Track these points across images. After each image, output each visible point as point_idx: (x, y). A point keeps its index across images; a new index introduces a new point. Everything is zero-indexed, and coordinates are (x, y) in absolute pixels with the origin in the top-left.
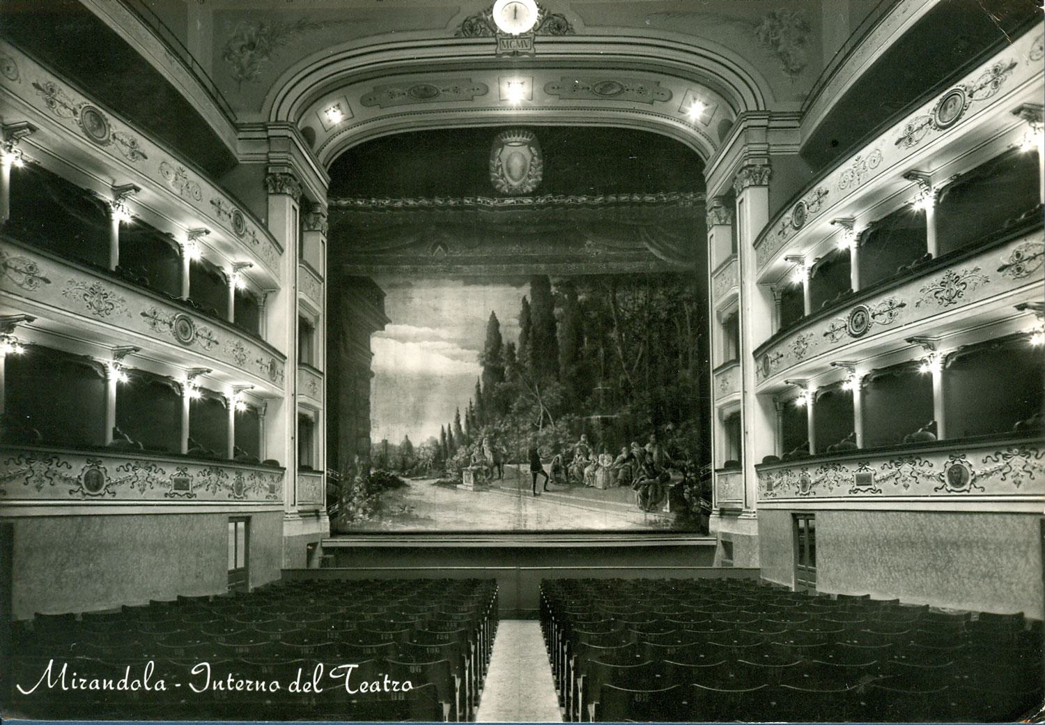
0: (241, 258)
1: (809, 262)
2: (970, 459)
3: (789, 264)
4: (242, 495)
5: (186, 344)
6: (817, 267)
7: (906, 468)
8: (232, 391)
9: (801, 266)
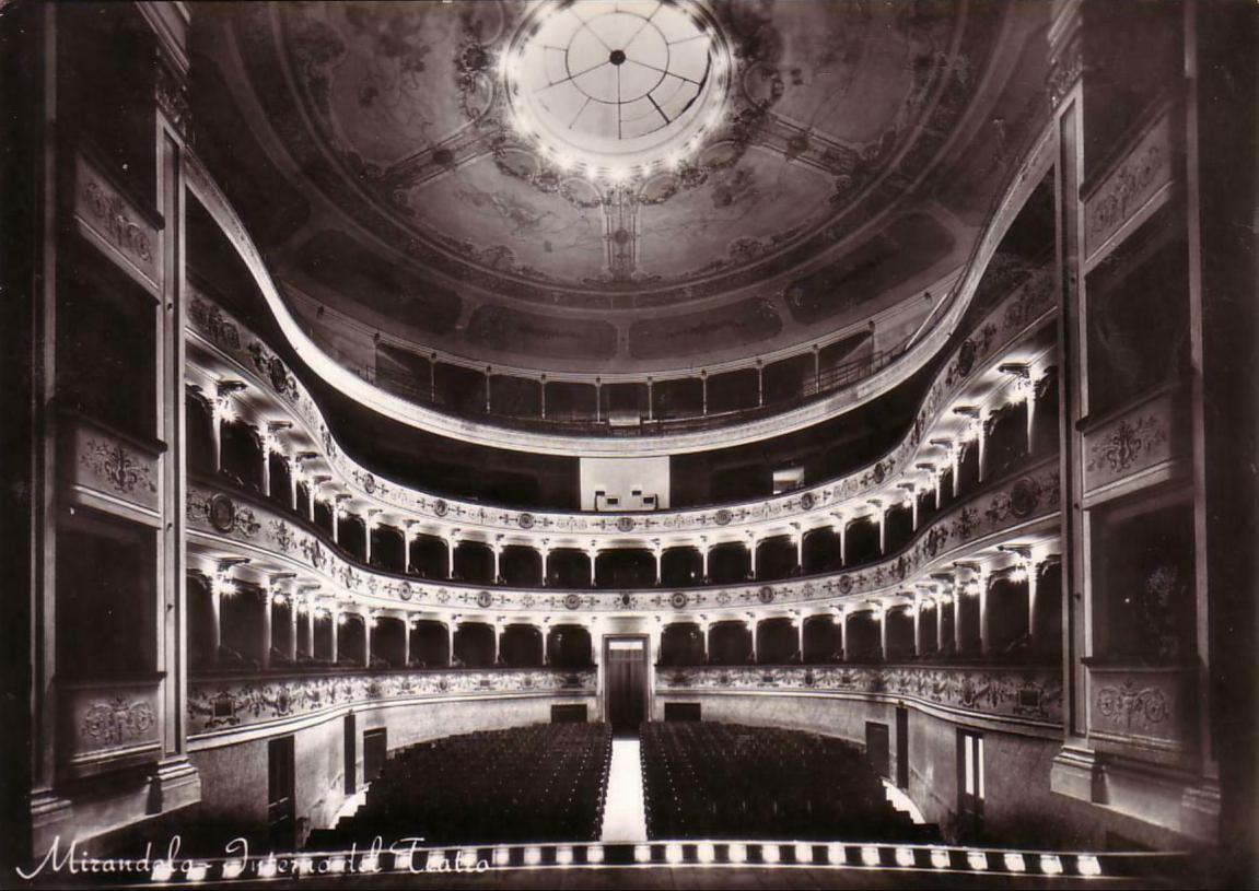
1: (985, 416)
3: (1008, 376)
4: (287, 711)
5: (222, 532)
7: (424, 679)
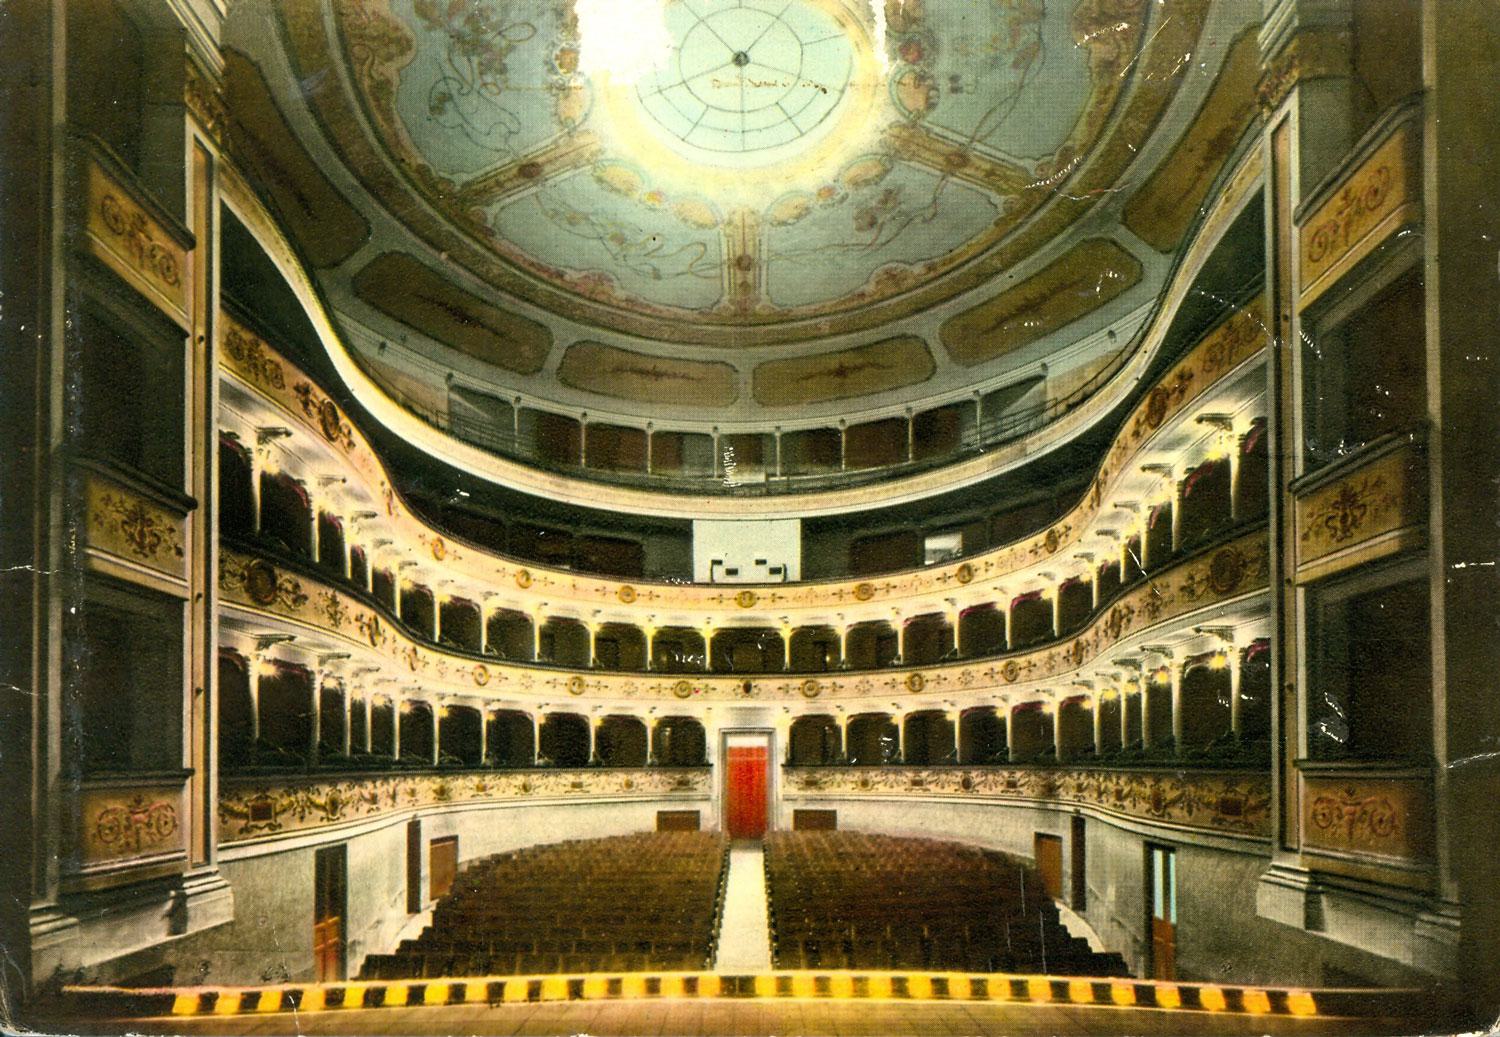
0: (273, 420)
1: (1180, 475)
2: (872, 774)
6: (1192, 482)
8: (317, 660)
9: (1225, 433)
